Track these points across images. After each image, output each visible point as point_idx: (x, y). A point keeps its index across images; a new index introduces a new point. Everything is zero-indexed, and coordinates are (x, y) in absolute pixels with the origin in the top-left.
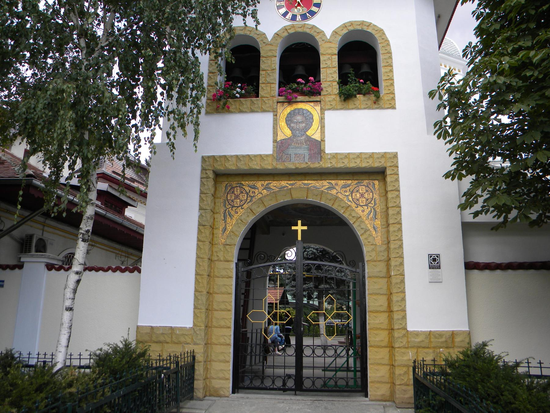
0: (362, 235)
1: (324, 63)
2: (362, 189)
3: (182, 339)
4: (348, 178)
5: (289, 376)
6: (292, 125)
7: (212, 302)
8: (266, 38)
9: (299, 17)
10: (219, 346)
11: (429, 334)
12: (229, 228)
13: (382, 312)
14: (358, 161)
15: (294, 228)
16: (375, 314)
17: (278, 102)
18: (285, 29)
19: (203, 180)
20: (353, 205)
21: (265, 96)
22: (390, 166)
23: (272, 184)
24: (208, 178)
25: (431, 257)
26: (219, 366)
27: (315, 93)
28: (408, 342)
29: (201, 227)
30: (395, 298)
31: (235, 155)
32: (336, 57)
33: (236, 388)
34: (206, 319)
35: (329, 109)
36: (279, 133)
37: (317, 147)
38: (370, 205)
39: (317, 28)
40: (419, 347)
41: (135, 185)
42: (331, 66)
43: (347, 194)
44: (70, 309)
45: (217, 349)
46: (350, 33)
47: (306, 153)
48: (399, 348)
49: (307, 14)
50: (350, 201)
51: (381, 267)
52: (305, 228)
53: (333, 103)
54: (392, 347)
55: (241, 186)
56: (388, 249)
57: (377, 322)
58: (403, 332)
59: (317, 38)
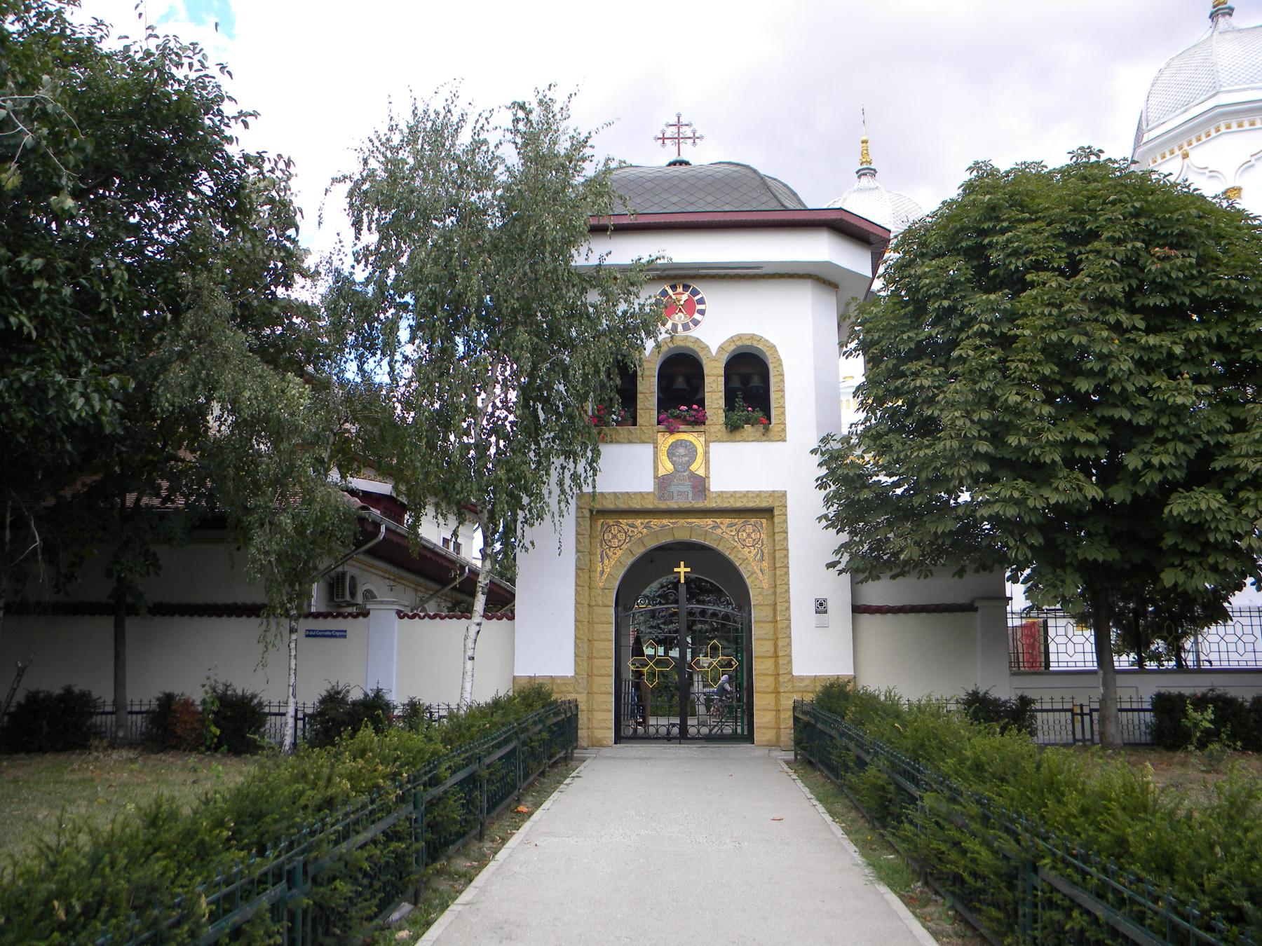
2: (749, 529)
3: (564, 688)
5: (674, 725)
12: (607, 570)
14: (745, 500)
20: (740, 546)
24: (584, 517)
26: (599, 717)
27: (698, 421)
30: (780, 643)
33: (619, 738)
36: (660, 466)
37: (700, 485)
44: (472, 658)
45: (599, 698)
47: (689, 489)
51: (768, 611)
53: (719, 435)
56: (775, 593)
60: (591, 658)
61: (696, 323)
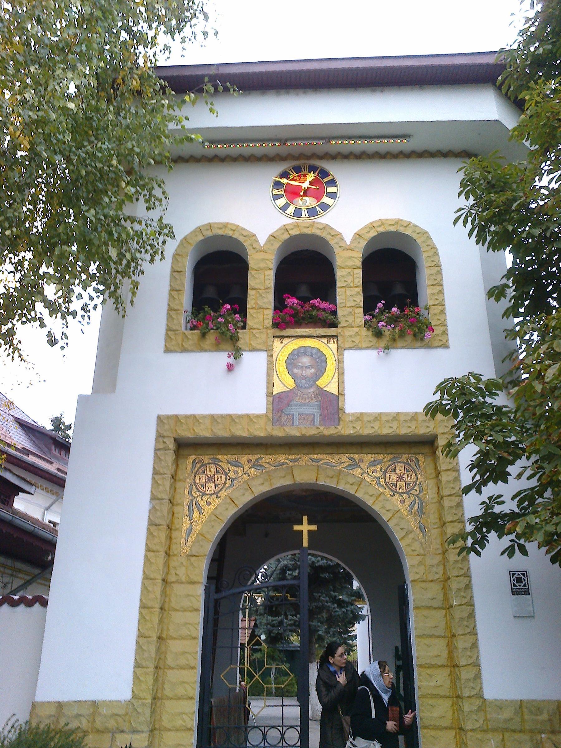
0: (403, 538)
1: (343, 279)
2: (400, 468)
4: (379, 451)
6: (295, 371)
7: (165, 653)
8: (257, 241)
9: (305, 213)
10: (172, 733)
11: (521, 706)
12: (197, 528)
13: (440, 666)
15: (296, 528)
16: (428, 671)
17: (274, 337)
18: (285, 229)
19: (158, 453)
20: (388, 492)
21: (255, 326)
22: (443, 433)
23: (264, 460)
24: (166, 449)
25: (513, 575)
28: (486, 720)
29: (153, 528)
31: (209, 415)
32: (360, 271)
34: (154, 685)
35: (350, 348)
37: (331, 405)
38: (412, 492)
39: (332, 229)
40: (507, 730)
41: (31, 459)
42: (352, 285)
43: (378, 475)
46: (381, 236)
48: (472, 730)
49: (318, 209)
50: (383, 486)
52: (314, 528)
54: (461, 729)
55: (216, 462)
57: (433, 683)
58: (478, 702)
59: (332, 243)
60: (159, 668)
61: (325, 207)
